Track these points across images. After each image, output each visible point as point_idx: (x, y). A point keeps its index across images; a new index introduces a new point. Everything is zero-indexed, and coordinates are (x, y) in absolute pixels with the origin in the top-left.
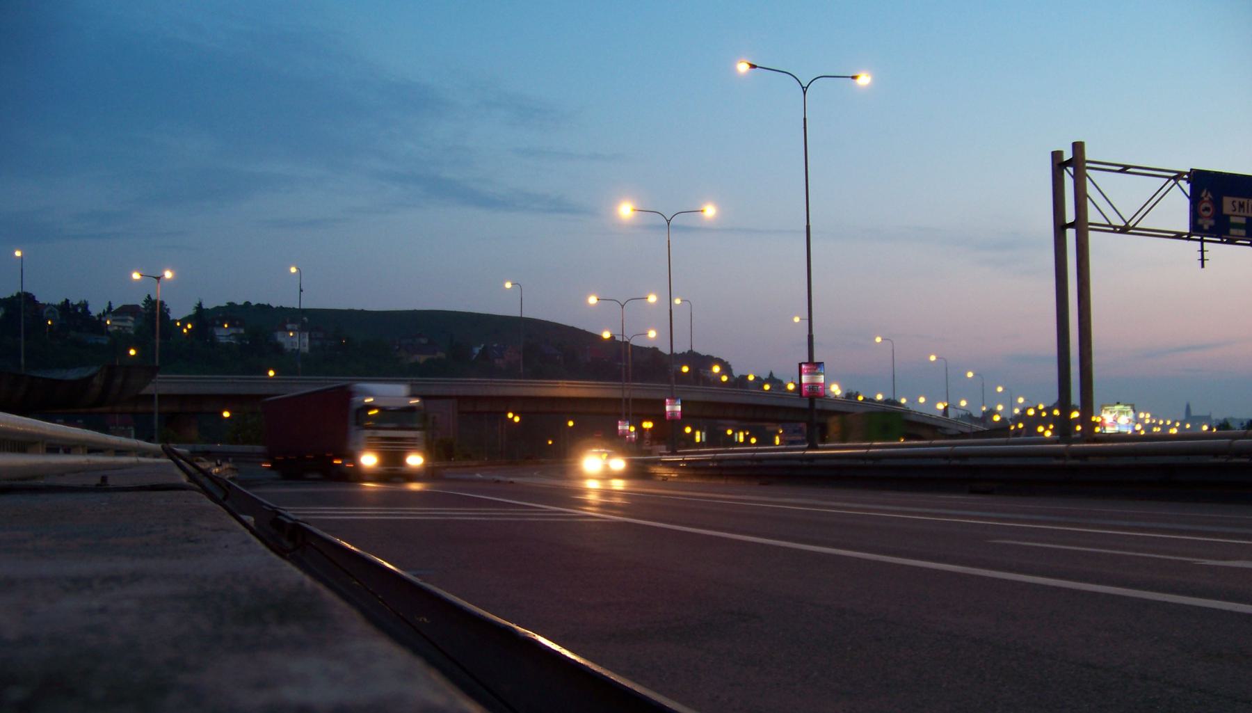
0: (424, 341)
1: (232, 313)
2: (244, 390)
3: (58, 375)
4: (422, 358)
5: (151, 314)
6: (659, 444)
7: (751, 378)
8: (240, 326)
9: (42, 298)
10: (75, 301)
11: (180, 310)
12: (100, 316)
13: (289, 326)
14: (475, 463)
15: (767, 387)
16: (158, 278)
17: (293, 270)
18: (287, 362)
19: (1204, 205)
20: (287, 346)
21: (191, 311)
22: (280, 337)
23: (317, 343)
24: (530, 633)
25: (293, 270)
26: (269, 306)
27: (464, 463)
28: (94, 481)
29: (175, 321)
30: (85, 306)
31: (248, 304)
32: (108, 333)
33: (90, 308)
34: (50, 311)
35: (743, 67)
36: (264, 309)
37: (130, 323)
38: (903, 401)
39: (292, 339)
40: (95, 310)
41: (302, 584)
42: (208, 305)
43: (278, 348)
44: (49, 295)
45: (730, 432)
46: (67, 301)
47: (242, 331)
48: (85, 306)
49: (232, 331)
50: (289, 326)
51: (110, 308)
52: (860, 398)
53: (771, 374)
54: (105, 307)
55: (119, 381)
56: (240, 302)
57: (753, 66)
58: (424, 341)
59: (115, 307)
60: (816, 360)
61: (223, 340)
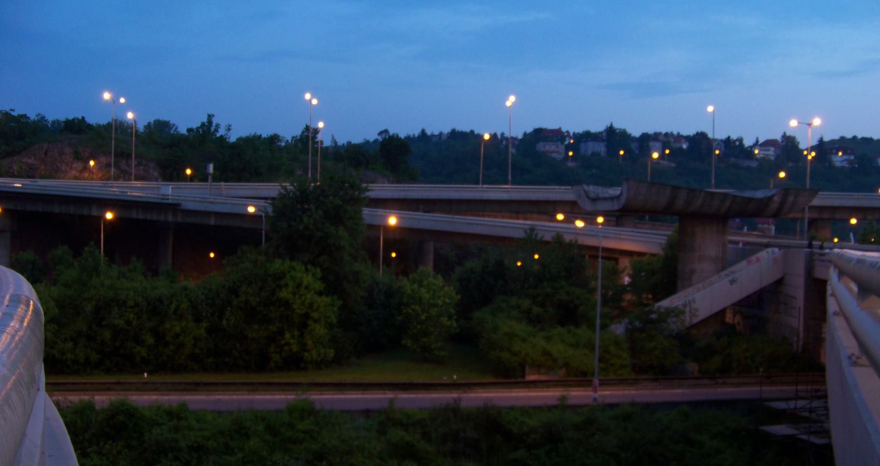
1: (843, 144)
3: (748, 194)
5: (788, 147)
8: (850, 154)
10: (734, 137)
11: (806, 142)
21: (814, 142)
24: (615, 392)
28: (846, 279)
30: (740, 140)
31: (855, 138)
32: (757, 160)
34: (718, 144)
36: (867, 141)
37: (771, 152)
40: (748, 143)
41: (110, 400)
46: (423, 131)
47: (852, 157)
48: (740, 140)
49: (846, 157)
51: (757, 141)
55: (791, 199)
56: (849, 136)
59: (761, 141)
61: (838, 164)
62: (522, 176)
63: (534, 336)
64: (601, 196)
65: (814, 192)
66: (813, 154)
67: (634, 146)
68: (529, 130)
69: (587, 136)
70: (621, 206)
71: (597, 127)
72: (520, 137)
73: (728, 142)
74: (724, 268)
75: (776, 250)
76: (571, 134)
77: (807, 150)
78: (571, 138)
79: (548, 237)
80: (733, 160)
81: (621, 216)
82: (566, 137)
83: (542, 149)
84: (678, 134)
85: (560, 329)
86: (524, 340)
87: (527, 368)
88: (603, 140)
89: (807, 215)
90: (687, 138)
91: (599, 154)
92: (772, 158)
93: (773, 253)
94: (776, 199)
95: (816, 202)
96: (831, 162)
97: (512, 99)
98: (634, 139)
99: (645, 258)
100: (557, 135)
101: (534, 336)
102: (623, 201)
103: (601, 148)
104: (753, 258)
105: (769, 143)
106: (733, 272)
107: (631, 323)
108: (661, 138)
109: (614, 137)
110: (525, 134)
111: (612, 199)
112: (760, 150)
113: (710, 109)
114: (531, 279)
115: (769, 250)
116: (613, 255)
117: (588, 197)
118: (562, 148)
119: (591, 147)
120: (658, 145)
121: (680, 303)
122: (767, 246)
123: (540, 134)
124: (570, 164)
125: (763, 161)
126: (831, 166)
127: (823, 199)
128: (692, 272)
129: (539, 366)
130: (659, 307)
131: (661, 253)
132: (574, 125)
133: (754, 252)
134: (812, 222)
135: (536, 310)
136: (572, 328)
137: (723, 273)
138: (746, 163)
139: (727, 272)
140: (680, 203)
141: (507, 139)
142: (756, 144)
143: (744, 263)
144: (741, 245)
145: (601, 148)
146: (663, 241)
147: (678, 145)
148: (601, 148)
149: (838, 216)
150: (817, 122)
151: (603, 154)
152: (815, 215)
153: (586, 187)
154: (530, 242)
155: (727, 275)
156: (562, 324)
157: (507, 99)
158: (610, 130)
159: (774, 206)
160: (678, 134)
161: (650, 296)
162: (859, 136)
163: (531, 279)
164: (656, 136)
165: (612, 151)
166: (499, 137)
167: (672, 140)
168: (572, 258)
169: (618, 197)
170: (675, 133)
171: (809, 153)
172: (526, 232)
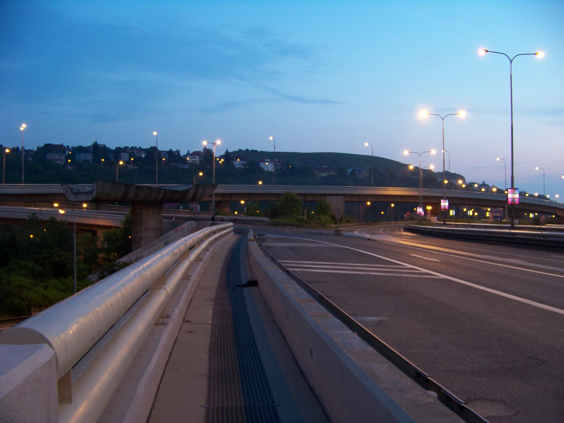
0: (326, 166)
2: (250, 191)
4: (325, 175)
6: (434, 216)
9: (160, 149)
10: (174, 150)
11: (217, 153)
12: (184, 156)
13: (266, 160)
14: (352, 224)
15: (483, 190)
16: (214, 144)
17: (271, 138)
18: (267, 177)
20: (265, 169)
21: (223, 153)
22: (262, 165)
23: (278, 167)
25: (271, 138)
26: (257, 151)
27: (347, 225)
29: (216, 158)
30: (178, 152)
32: (188, 164)
33: (180, 153)
35: (481, 52)
37: (197, 159)
38: (548, 196)
39: (268, 166)
40: (183, 153)
42: (230, 151)
43: (261, 170)
44: (163, 147)
45: (465, 210)
47: (245, 162)
48: (178, 152)
49: (242, 162)
50: (266, 160)
51: (189, 152)
52: (527, 195)
53: (484, 182)
54: (187, 152)
55: (200, 191)
56: (244, 149)
57: (487, 51)
58: (326, 166)
59: (191, 152)
60: (515, 187)
61: (237, 166)
62: (33, 176)
63: (36, 286)
64: (81, 191)
65: (215, 186)
66: (222, 160)
67: (111, 155)
68: (41, 145)
69: (80, 149)
70: (93, 198)
71: (87, 143)
72: (35, 149)
73: (170, 152)
74: (161, 235)
75: (193, 222)
76: (70, 148)
77: (218, 158)
78: (70, 150)
79: (46, 218)
80: (173, 164)
81: (97, 202)
82: (66, 149)
83: (50, 158)
84: (140, 147)
85: (55, 281)
86: (29, 289)
87: (32, 308)
88: (91, 152)
89: (214, 199)
90: (146, 151)
91: (88, 161)
92: (198, 163)
93: (192, 224)
94: (191, 191)
95: (217, 191)
96: (233, 165)
97: (24, 126)
98: (112, 151)
99: (112, 230)
100: (60, 149)
101: (36, 286)
102: (94, 194)
103: (90, 157)
104: (179, 228)
105: (196, 153)
106: (167, 237)
107: (101, 273)
108: (128, 150)
109: (98, 150)
110: (38, 148)
111: (87, 193)
112: (190, 158)
113: (155, 133)
114: (34, 247)
115: (189, 222)
116: (92, 230)
117: (73, 192)
118: (63, 157)
119: (83, 157)
120: (126, 155)
121: (134, 258)
122: (188, 220)
123: (48, 148)
124: (69, 168)
125: (192, 164)
126: (233, 168)
127: (221, 189)
128: (141, 238)
129: (40, 306)
130: (120, 262)
131: (122, 226)
132: (72, 142)
133: (180, 224)
134: (218, 204)
135: (38, 268)
136: (63, 279)
137: (160, 239)
138: (182, 166)
139: (163, 237)
140: (131, 196)
141: (25, 151)
142: (188, 154)
143: (173, 231)
144: (174, 219)
145: (90, 157)
146: (123, 218)
147: (139, 155)
148: (89, 157)
149: (234, 199)
150: (218, 142)
151: (90, 161)
152: (220, 199)
153: (71, 186)
154: (34, 223)
155: (163, 239)
156: (56, 277)
157: (21, 126)
158: (95, 145)
159: (190, 195)
160: (140, 147)
161: (116, 254)
162: (250, 149)
163: (34, 247)
164: (125, 149)
165: (97, 159)
166: (20, 149)
167: (135, 152)
168: (60, 231)
169: (91, 192)
170: (138, 147)
171: (220, 160)
172: (29, 216)
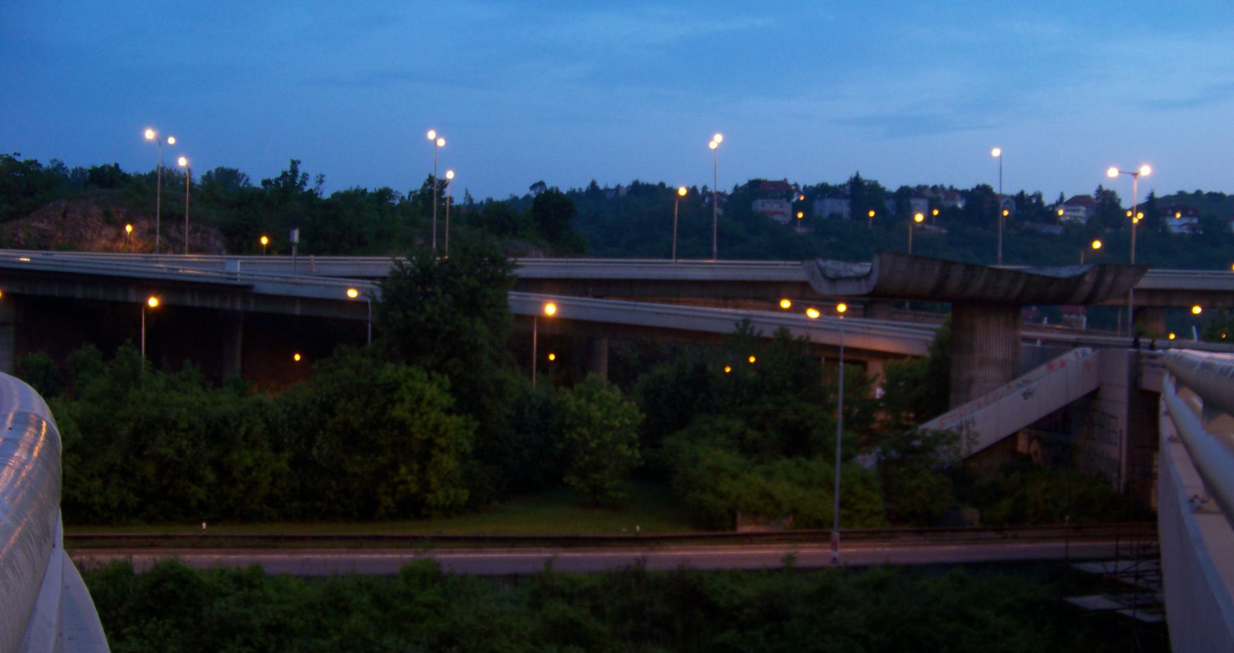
1: (1182, 202)
3: (1049, 272)
5: (1105, 205)
7: (683, 192)
8: (1192, 216)
10: (1029, 192)
11: (1130, 198)
19: (452, 492)
21: (1141, 199)
28: (1186, 391)
30: (1038, 196)
31: (1198, 193)
32: (1061, 224)
34: (1007, 202)
36: (1216, 198)
37: (1081, 213)
40: (1048, 200)
47: (1195, 221)
48: (1038, 196)
49: (1186, 220)
51: (1062, 198)
55: (1109, 278)
56: (1191, 190)
59: (1067, 197)
61: (1175, 230)
62: (732, 246)
63: (749, 471)
64: (843, 274)
65: (1141, 270)
66: (1140, 216)
67: (889, 204)
68: (742, 182)
69: (823, 191)
70: (871, 289)
71: (838, 178)
72: (729, 191)
73: (1020, 198)
74: (1015, 376)
75: (1088, 350)
76: (801, 188)
77: (1131, 209)
78: (801, 194)
79: (768, 332)
80: (1027, 224)
81: (870, 303)
82: (793, 192)
83: (761, 209)
84: (951, 187)
85: (785, 461)
86: (734, 477)
87: (739, 516)
88: (845, 197)
89: (1132, 301)
90: (964, 194)
91: (840, 216)
92: (1083, 222)
93: (1084, 354)
94: (1088, 278)
95: (1144, 283)
96: (1165, 227)
97: (718, 139)
98: (889, 195)
99: (905, 362)
100: (782, 189)
101: (749, 471)
102: (873, 281)
103: (843, 208)
104: (1056, 361)
105: (1078, 201)
106: (1028, 382)
107: (884, 453)
108: (926, 193)
109: (860, 192)
110: (736, 188)
111: (858, 278)
112: (1066, 211)
113: (996, 152)
114: (745, 391)
115: (1079, 350)
116: (859, 358)
117: (825, 277)
118: (788, 208)
119: (828, 207)
120: (923, 203)
121: (954, 424)
122: (1075, 344)
123: (757, 188)
124: (799, 230)
125: (1070, 225)
126: (1166, 232)
127: (1154, 279)
128: (971, 381)
129: (756, 513)
130: (925, 431)
131: (927, 354)
132: (804, 175)
133: (1057, 353)
134: (1139, 312)
135: (752, 434)
136: (803, 460)
137: (1014, 383)
138: (1047, 229)
139: (1019, 381)
140: (953, 285)
141: (711, 195)
142: (1060, 202)
143: (1043, 369)
144: (1038, 343)
145: (843, 208)
146: (930, 337)
147: (951, 204)
148: (843, 207)
149: (1175, 302)
150: (1145, 171)
151: (845, 216)
152: (1143, 302)
153: (821, 262)
154: (744, 340)
155: (1020, 386)
156: (789, 454)
157: (711, 139)
158: (856, 182)
159: (1085, 289)
160: (951, 187)
161: (911, 415)
162: (1205, 191)
163: (745, 391)
164: (920, 191)
165: (858, 211)
166: (700, 192)
167: (942, 196)
168: (802, 362)
169: (866, 277)
170: (947, 186)
171: (1135, 215)
172: (737, 325)
